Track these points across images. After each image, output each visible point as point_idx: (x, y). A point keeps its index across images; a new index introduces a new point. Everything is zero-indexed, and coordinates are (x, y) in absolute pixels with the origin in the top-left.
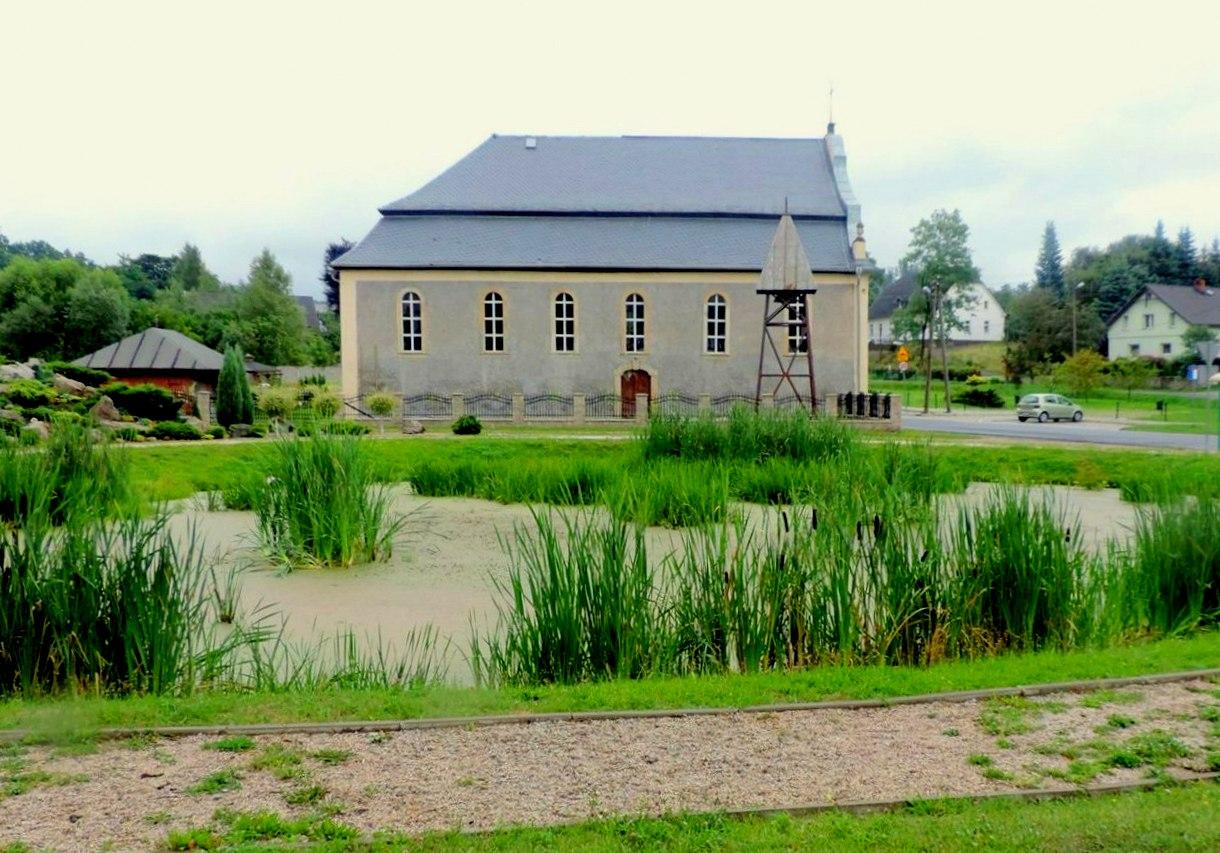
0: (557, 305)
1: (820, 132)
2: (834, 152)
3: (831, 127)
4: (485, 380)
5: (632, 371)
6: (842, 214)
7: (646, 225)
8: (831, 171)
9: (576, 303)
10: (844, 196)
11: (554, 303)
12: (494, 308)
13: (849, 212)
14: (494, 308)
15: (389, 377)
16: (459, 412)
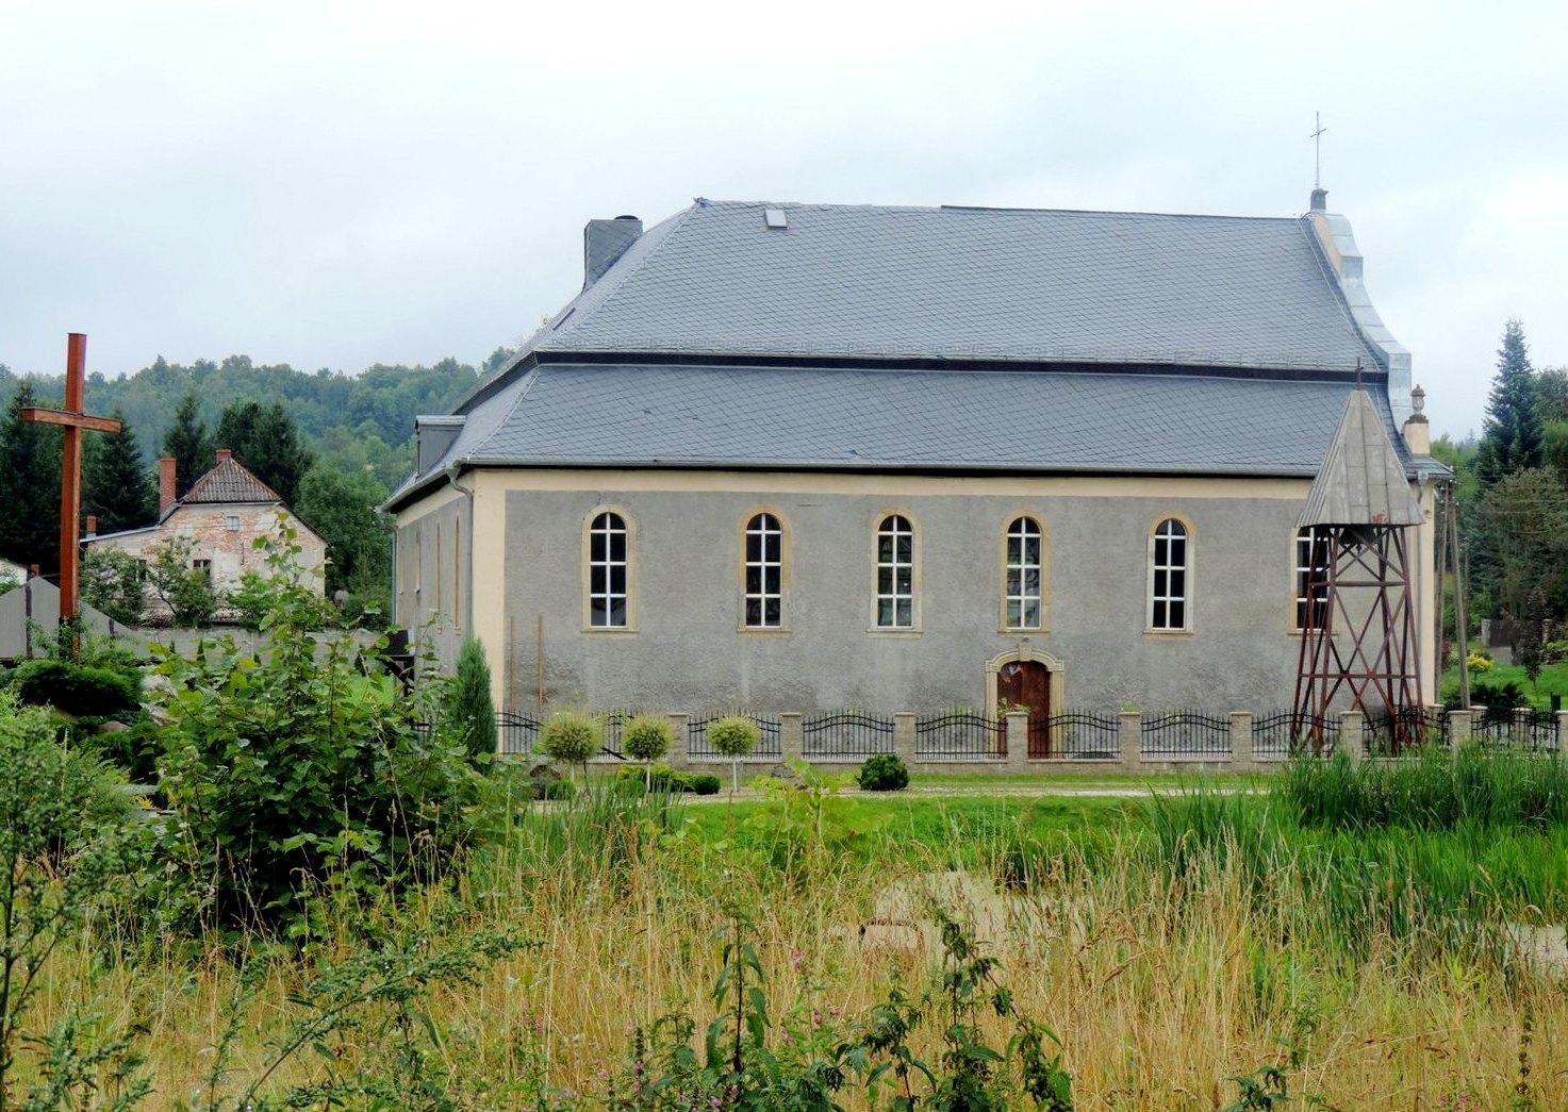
0: (1158, 541)
1: (1299, 207)
2: (1335, 250)
3: (1318, 198)
4: (745, 683)
5: (1016, 663)
6: (1379, 370)
7: (1029, 384)
8: (1334, 282)
9: (917, 535)
10: (1370, 332)
11: (588, 533)
12: (765, 543)
13: (1392, 366)
14: (765, 543)
15: (562, 677)
16: (867, 745)
